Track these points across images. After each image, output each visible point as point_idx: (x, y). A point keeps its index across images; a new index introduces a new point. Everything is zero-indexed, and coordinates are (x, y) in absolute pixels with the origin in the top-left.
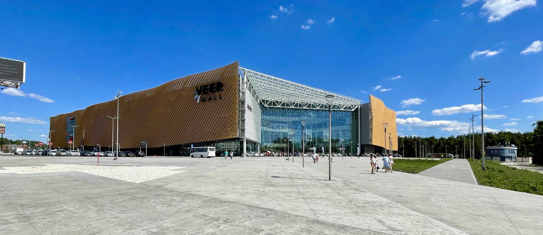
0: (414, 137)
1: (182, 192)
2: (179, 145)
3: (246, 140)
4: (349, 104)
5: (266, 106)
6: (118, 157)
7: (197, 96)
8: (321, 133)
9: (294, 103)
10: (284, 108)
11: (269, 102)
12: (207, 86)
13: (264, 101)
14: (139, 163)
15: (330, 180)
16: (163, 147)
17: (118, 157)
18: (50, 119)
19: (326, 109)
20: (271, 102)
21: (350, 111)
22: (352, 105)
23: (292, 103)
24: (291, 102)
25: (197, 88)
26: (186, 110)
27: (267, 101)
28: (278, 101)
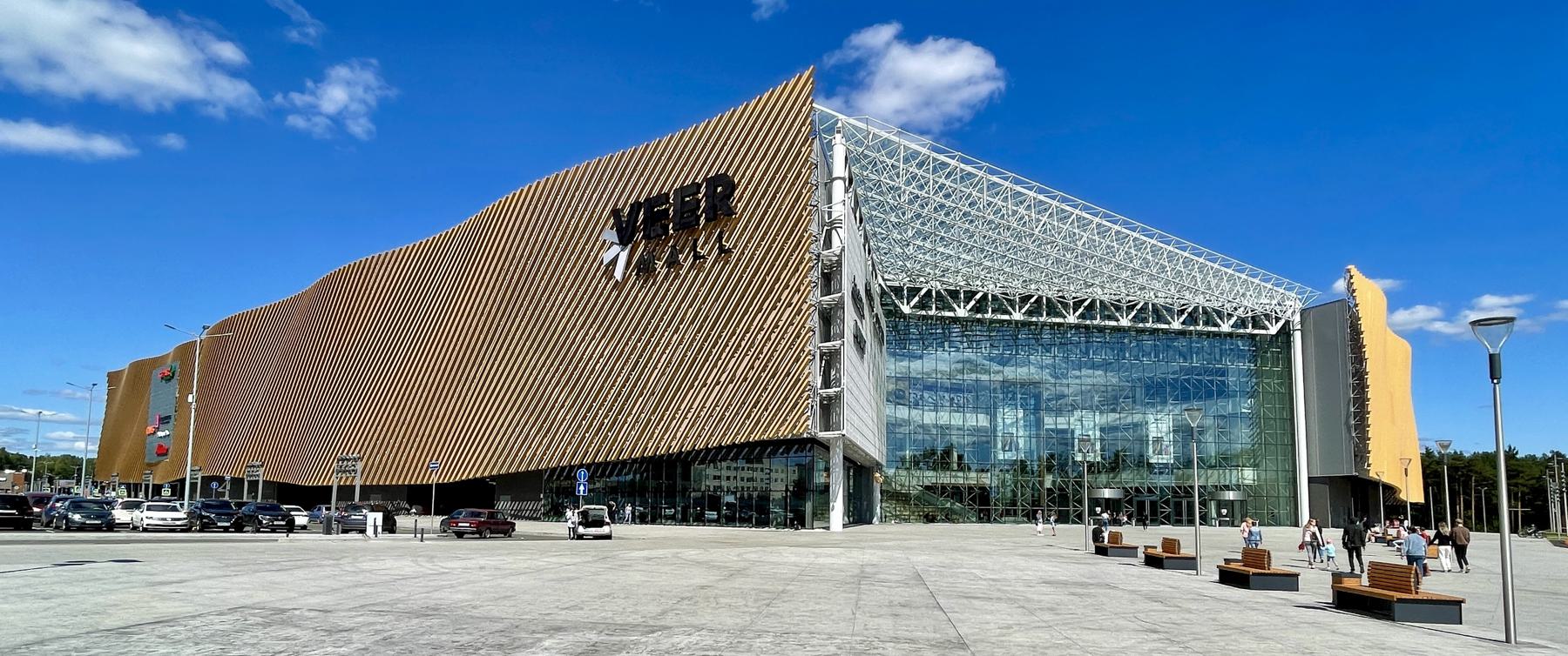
3: (845, 458)
5: (906, 309)
7: (616, 249)
13: (898, 291)
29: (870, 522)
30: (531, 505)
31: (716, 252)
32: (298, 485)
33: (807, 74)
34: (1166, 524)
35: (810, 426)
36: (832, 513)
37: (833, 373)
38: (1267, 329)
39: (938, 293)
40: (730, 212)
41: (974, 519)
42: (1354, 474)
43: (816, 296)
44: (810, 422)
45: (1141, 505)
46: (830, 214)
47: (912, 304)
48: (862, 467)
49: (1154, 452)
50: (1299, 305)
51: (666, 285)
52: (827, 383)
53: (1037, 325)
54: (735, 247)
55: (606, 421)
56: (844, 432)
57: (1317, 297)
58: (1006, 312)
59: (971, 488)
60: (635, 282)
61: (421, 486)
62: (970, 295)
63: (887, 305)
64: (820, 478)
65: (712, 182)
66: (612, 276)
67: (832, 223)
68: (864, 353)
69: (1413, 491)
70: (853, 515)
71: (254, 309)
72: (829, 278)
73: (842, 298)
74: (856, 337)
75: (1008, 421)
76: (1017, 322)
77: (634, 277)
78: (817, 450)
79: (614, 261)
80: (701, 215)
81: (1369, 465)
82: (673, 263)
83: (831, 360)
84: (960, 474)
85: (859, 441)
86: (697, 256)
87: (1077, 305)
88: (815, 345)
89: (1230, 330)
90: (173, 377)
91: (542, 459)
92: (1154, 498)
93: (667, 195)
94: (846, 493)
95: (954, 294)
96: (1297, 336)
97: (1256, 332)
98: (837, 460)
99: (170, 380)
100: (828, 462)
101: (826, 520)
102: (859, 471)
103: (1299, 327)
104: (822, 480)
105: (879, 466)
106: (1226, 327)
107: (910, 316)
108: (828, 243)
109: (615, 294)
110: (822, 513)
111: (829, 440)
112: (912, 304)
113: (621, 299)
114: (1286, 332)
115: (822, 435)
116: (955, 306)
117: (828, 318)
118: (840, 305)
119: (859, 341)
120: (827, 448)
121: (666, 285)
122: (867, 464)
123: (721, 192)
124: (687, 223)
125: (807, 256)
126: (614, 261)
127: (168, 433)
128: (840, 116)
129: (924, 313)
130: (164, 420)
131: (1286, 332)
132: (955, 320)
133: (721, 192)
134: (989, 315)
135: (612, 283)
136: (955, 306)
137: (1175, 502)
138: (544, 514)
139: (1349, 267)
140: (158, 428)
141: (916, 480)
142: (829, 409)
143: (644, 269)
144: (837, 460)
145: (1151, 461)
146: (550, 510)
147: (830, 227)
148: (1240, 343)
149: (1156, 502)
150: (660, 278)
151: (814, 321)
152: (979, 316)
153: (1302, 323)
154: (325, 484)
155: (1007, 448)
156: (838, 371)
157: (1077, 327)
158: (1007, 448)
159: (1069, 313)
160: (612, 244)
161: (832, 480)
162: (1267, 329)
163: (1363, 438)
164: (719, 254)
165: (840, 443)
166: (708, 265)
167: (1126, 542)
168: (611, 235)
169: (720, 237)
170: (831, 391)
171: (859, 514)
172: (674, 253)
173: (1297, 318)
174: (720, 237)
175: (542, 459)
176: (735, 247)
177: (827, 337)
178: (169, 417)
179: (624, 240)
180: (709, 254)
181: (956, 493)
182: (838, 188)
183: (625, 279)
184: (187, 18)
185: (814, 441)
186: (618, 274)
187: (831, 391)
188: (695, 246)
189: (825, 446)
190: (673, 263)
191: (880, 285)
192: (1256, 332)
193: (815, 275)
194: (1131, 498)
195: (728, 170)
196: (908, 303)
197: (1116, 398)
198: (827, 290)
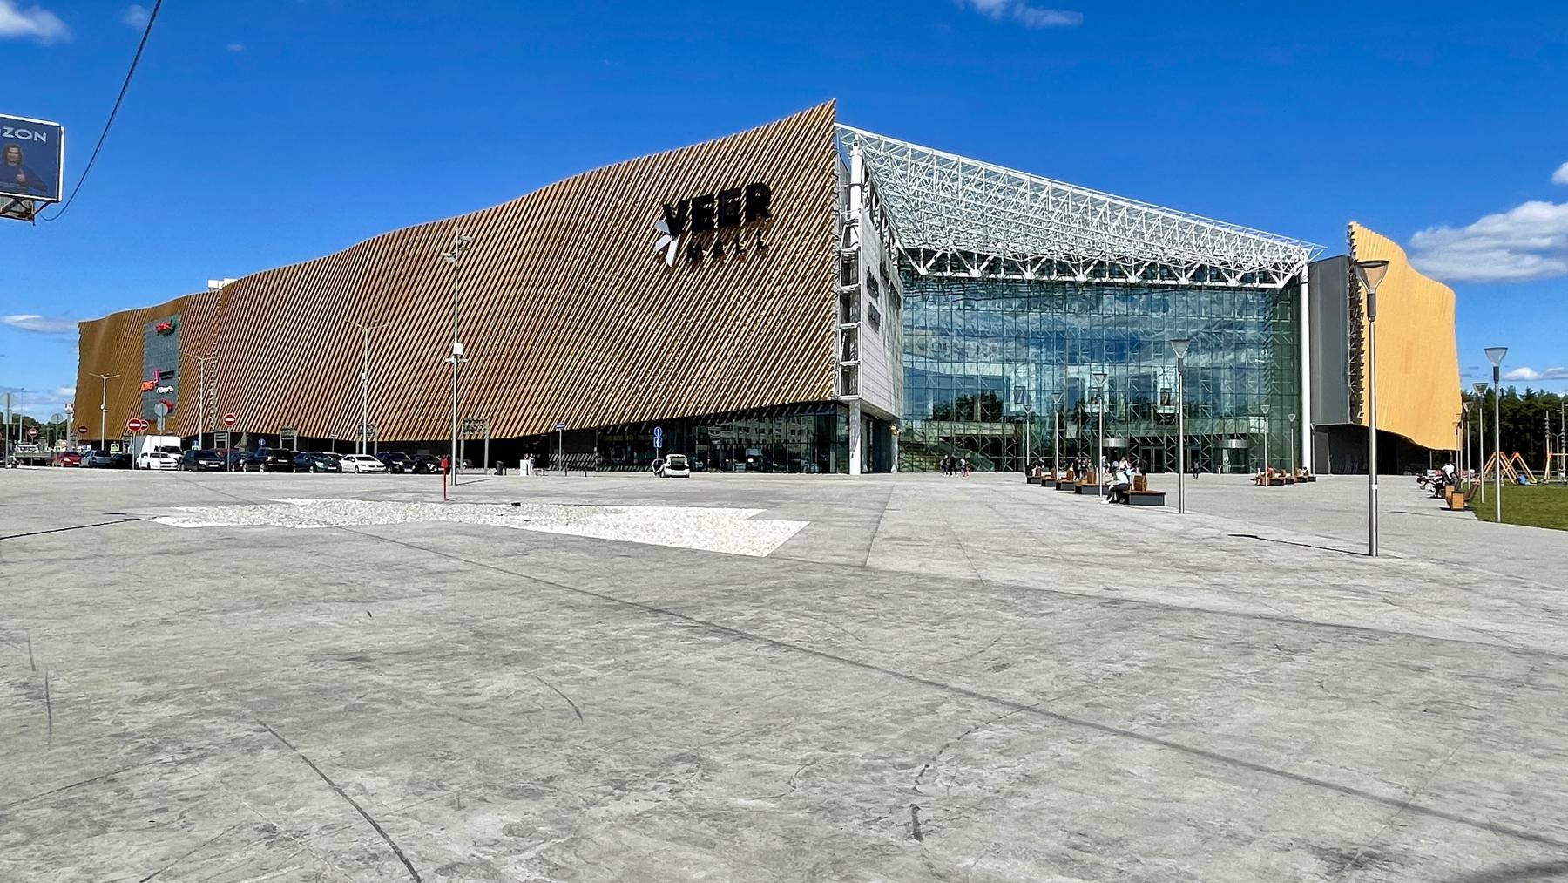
0: (1524, 393)
1: (1026, 589)
2: (585, 429)
3: (862, 413)
4: (1259, 259)
5: (923, 271)
6: (1379, 472)
7: (666, 239)
8: (1148, 381)
9: (1037, 260)
10: (995, 280)
11: (938, 255)
12: (710, 198)
13: (914, 253)
14: (772, 494)
15: (1371, 554)
16: (483, 441)
17: (1379, 472)
18: (1458, 407)
19: (1167, 282)
20: (944, 255)
21: (1263, 290)
22: (1276, 266)
23: (1028, 259)
24: (1026, 257)
25: (667, 208)
26: (408, 275)
27: (929, 254)
28: (973, 254)
29: (889, 471)
30: (585, 457)
31: (755, 246)
32: (324, 439)
33: (830, 104)
34: (1170, 471)
35: (835, 391)
36: (851, 460)
37: (852, 346)
38: (1274, 282)
39: (953, 255)
40: (766, 214)
41: (992, 469)
42: (1350, 422)
43: (838, 286)
44: (833, 389)
45: (1147, 454)
46: (849, 217)
47: (929, 265)
48: (881, 421)
49: (1162, 403)
50: (1305, 259)
51: (712, 272)
52: (847, 357)
53: (1048, 284)
54: (771, 244)
55: (728, 394)
56: (861, 396)
57: (1322, 251)
58: (1018, 271)
59: (984, 439)
60: (684, 268)
61: (443, 441)
62: (983, 258)
63: (905, 266)
64: (841, 431)
65: (751, 189)
66: (664, 260)
67: (851, 222)
68: (878, 324)
69: (1442, 434)
70: (873, 464)
71: (287, 267)
72: (849, 266)
73: (859, 289)
74: (870, 316)
75: (1021, 375)
76: (1029, 281)
77: (683, 262)
78: (840, 411)
79: (666, 248)
80: (742, 214)
81: (1361, 415)
82: (718, 253)
83: (850, 336)
84: (987, 425)
85: (875, 401)
86: (738, 248)
87: (1087, 264)
88: (838, 325)
89: (1238, 284)
90: (173, 331)
91: (603, 417)
92: (1194, 447)
93: (711, 196)
94: (865, 445)
95: (968, 255)
96: (1305, 289)
97: (1264, 286)
98: (855, 416)
99: (167, 334)
100: (848, 419)
101: (845, 469)
102: (878, 425)
103: (1307, 280)
104: (844, 432)
105: (894, 420)
106: (1233, 282)
107: (926, 278)
108: (847, 244)
109: (666, 276)
110: (844, 466)
111: (849, 401)
112: (929, 265)
113: (671, 282)
114: (1294, 284)
115: (843, 398)
116: (969, 267)
117: (847, 301)
118: (858, 291)
119: (874, 320)
120: (848, 407)
121: (712, 272)
122: (886, 418)
123: (759, 199)
124: (730, 220)
125: (831, 255)
126: (666, 248)
127: (172, 389)
128: (858, 131)
129: (939, 274)
130: (165, 376)
131: (1294, 284)
132: (971, 279)
133: (759, 199)
134: (1001, 276)
135: (663, 267)
136: (969, 267)
137: (1143, 451)
138: (598, 465)
139: (1351, 224)
140: (157, 384)
141: (935, 433)
142: (848, 375)
143: (694, 255)
144: (855, 416)
145: (1087, 410)
146: (603, 462)
147: (849, 225)
148: (1249, 296)
149: (1198, 451)
150: (706, 266)
151: (837, 307)
152: (992, 276)
153: (1309, 276)
154: (503, 437)
155: (1019, 401)
156: (856, 345)
157: (1087, 284)
158: (1019, 401)
159: (1079, 272)
160: (662, 234)
161: (852, 434)
162: (1274, 282)
163: (1357, 389)
164: (758, 249)
165: (858, 404)
166: (748, 257)
167: (1150, 488)
168: (662, 226)
169: (759, 234)
170: (851, 363)
171: (878, 462)
172: (719, 245)
173: (1305, 271)
174: (759, 234)
175: (603, 417)
176: (771, 244)
177: (847, 319)
178: (173, 373)
179: (675, 229)
180: (749, 248)
181: (970, 442)
182: (855, 191)
183: (675, 265)
184: (1499, 867)
185: (837, 403)
186: (670, 259)
187: (851, 363)
188: (737, 241)
189: (846, 405)
190: (718, 253)
191: (898, 249)
192: (1264, 286)
193: (838, 268)
194: (1137, 448)
195: (762, 179)
196: (924, 265)
197: (1123, 346)
198: (847, 282)
